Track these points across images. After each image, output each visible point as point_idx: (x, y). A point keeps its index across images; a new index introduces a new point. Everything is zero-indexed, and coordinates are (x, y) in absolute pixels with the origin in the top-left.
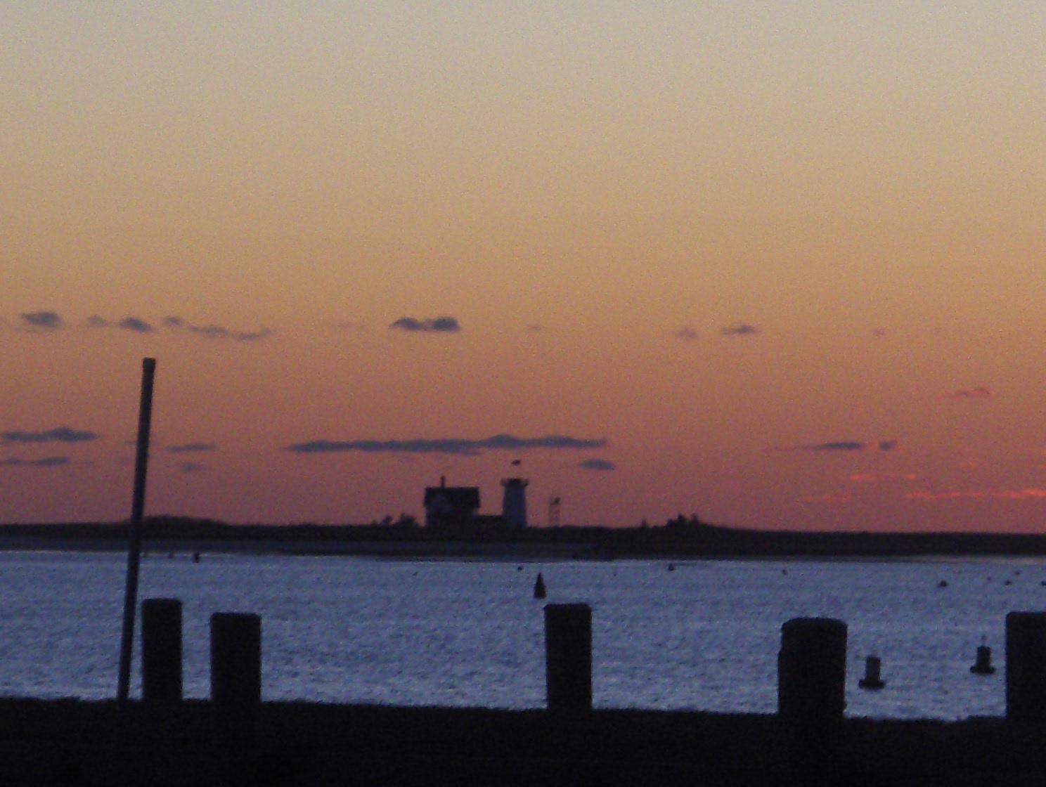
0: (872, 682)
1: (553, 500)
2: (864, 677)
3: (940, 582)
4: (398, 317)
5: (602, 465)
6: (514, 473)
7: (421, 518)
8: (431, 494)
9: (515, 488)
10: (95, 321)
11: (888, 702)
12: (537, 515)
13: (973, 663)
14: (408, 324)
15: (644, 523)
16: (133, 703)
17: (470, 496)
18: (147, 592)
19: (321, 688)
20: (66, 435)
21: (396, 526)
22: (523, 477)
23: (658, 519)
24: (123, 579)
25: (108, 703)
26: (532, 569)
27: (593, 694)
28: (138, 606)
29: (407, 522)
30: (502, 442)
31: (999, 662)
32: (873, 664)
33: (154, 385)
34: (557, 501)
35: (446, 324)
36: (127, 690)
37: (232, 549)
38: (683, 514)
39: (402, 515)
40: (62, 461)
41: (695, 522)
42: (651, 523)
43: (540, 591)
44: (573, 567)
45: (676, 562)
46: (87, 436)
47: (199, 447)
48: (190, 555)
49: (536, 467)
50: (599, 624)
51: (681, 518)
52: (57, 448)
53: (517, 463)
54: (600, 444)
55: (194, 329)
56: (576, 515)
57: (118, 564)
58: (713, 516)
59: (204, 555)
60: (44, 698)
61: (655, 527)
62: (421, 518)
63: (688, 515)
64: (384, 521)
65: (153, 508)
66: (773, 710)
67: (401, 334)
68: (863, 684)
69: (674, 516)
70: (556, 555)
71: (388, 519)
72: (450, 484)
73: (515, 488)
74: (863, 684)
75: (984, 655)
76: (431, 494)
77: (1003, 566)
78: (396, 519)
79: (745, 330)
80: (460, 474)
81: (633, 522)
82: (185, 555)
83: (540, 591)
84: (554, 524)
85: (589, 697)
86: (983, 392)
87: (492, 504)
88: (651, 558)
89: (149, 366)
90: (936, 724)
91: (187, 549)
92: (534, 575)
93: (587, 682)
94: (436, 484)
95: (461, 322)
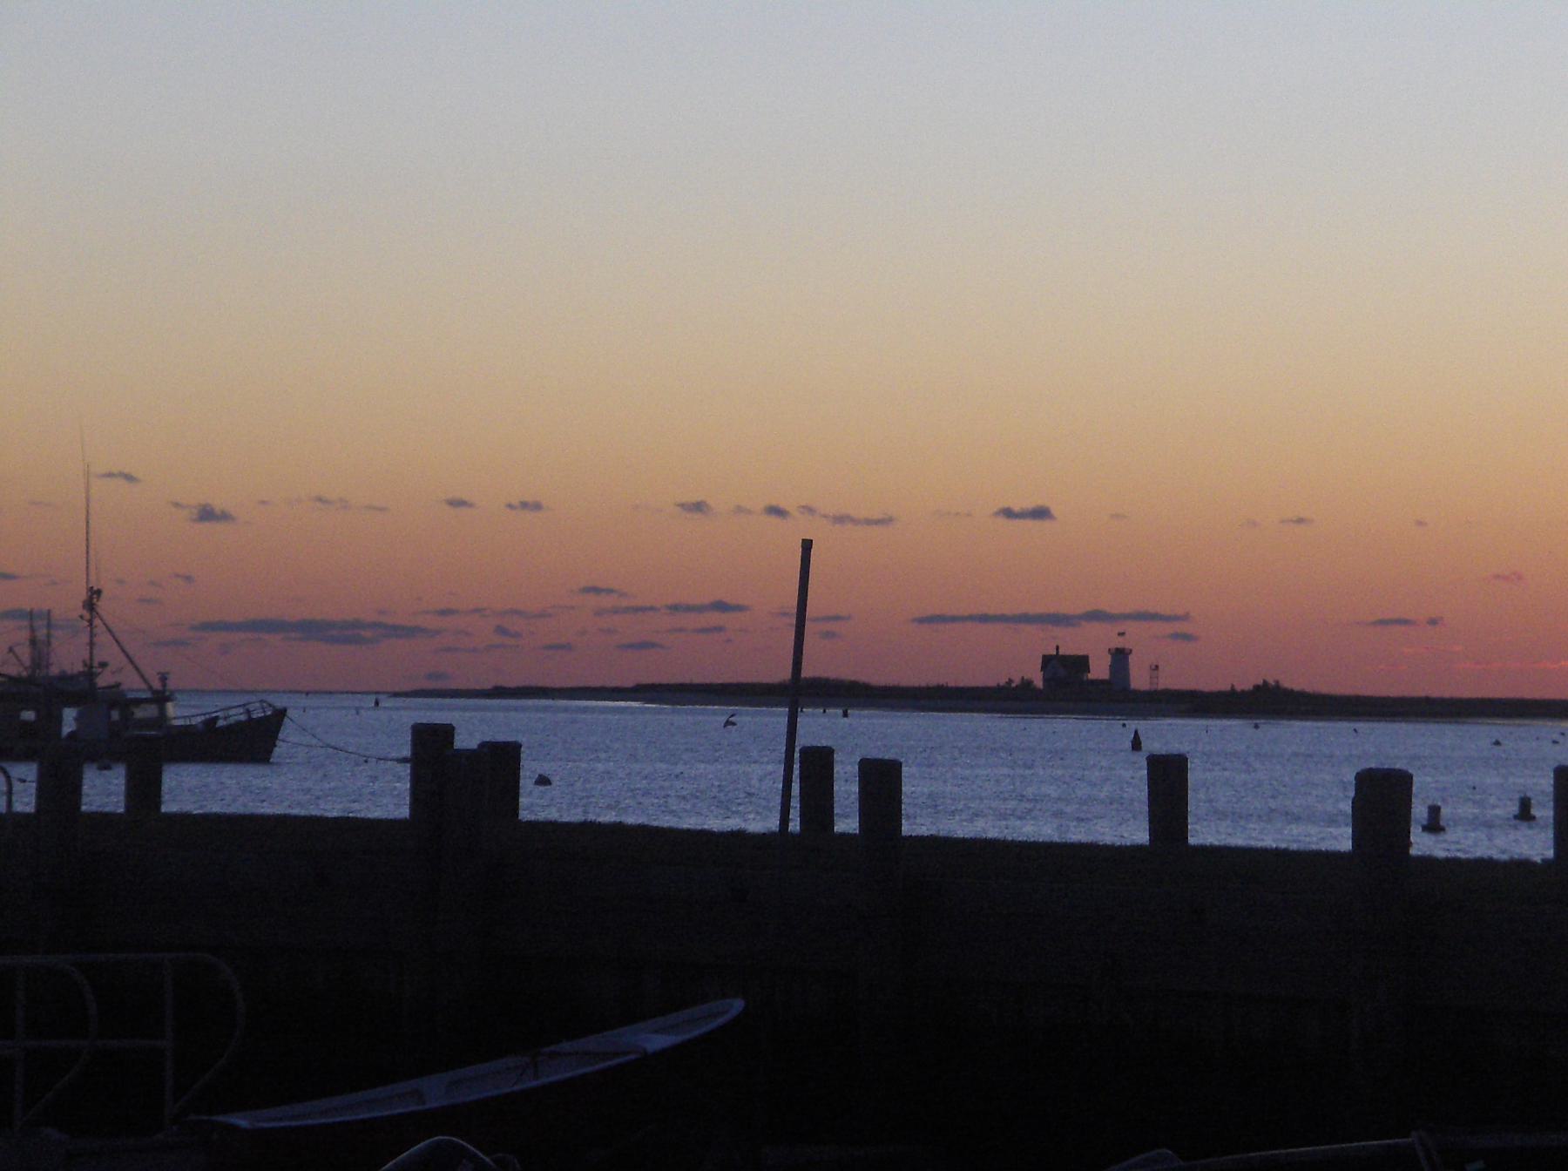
0: (1434, 825)
1: (1153, 667)
3: (1494, 740)
5: (1187, 637)
6: (1119, 643)
7: (1039, 683)
8: (1047, 661)
9: (1120, 657)
10: (739, 510)
12: (1139, 680)
14: (1008, 513)
17: (1082, 663)
18: (802, 741)
19: (356, 806)
20: (721, 606)
22: (1127, 647)
23: (1245, 684)
24: (784, 729)
25: (763, 839)
26: (1133, 724)
28: (797, 755)
29: (1027, 684)
30: (1096, 616)
31: (1544, 812)
32: (1434, 811)
34: (1157, 667)
35: (1041, 513)
37: (879, 707)
39: (1023, 678)
40: (720, 629)
42: (1239, 688)
43: (1136, 745)
44: (1170, 724)
45: (1262, 721)
46: (739, 608)
47: (837, 618)
48: (840, 711)
49: (1138, 638)
50: (1196, 775)
52: (715, 618)
53: (1121, 634)
54: (1185, 617)
55: (825, 516)
56: (1170, 680)
57: (777, 718)
61: (1243, 691)
62: (1039, 683)
63: (1271, 682)
65: (807, 672)
66: (121, 810)
67: (1002, 521)
69: (1260, 682)
70: (1145, 715)
71: (1011, 681)
73: (1120, 657)
74: (1426, 828)
76: (1047, 661)
78: (1017, 682)
79: (1300, 521)
80: (1071, 643)
81: (1223, 686)
82: (542, 716)
83: (1136, 745)
84: (1154, 687)
87: (1100, 669)
88: (1243, 718)
89: (807, 546)
91: (836, 706)
95: (1055, 511)
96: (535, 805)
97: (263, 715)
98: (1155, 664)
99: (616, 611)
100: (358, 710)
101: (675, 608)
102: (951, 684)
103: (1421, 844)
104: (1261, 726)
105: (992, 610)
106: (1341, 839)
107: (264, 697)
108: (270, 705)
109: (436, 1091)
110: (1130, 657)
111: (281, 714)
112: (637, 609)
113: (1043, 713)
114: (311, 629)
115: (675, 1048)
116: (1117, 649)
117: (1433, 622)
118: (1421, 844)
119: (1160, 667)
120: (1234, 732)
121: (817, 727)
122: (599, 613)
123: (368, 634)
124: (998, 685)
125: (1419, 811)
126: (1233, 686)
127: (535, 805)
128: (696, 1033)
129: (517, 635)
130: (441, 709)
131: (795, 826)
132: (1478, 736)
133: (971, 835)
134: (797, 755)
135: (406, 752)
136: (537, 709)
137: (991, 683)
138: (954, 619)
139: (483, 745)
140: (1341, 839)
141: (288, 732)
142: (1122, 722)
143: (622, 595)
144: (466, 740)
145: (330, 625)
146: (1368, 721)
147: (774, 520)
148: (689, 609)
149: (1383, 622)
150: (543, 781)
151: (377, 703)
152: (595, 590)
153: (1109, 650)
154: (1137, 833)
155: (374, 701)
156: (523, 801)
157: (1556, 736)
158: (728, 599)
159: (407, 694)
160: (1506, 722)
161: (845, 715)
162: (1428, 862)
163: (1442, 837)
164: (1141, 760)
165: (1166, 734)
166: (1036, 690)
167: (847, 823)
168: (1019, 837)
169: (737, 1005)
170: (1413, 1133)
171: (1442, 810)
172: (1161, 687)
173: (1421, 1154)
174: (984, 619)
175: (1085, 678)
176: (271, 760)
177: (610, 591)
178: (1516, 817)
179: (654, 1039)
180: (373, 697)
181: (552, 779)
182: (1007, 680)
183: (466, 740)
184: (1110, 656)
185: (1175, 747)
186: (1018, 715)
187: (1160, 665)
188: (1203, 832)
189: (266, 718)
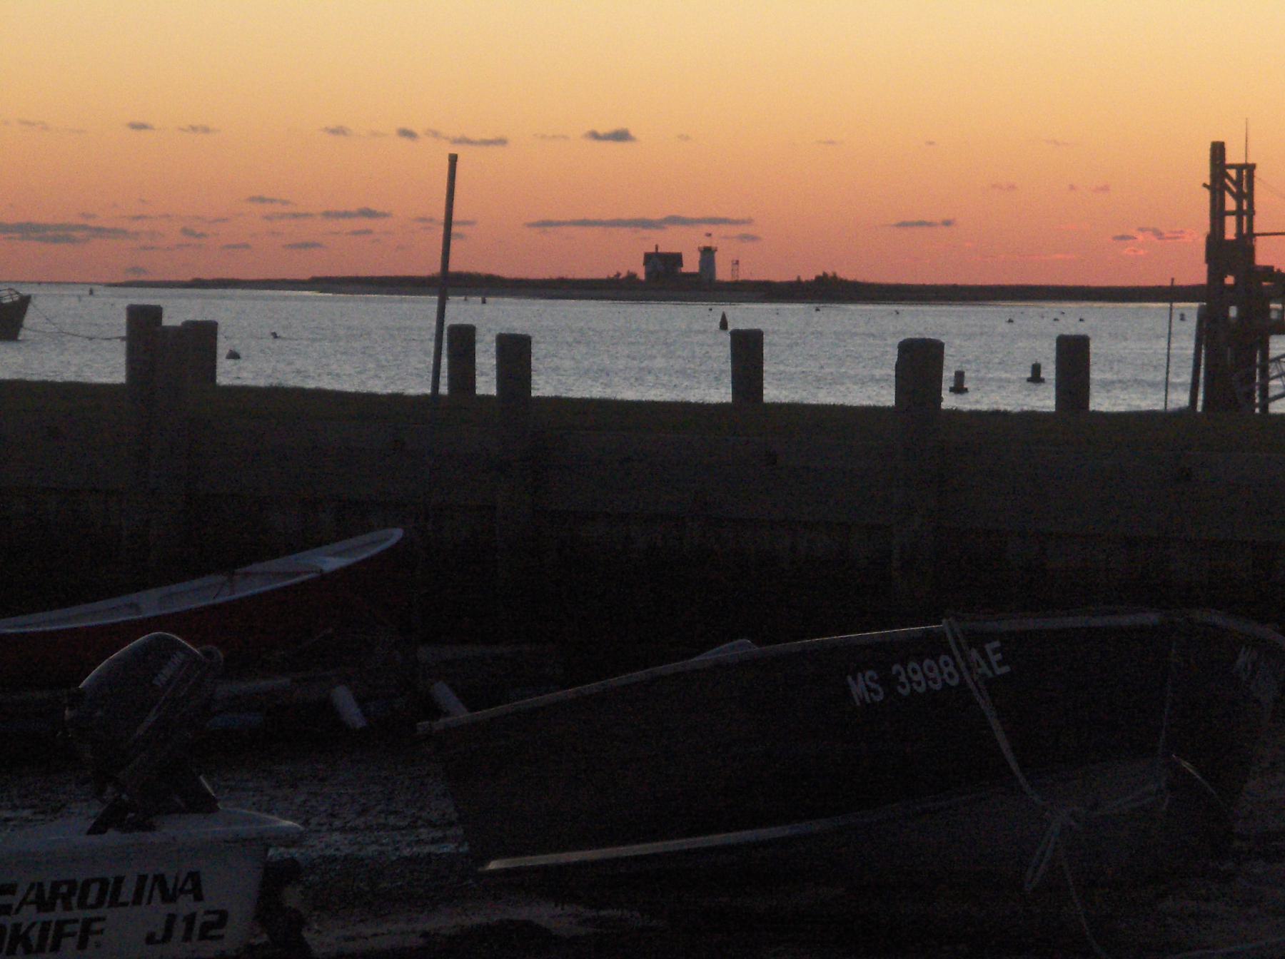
0: (959, 389)
2: (953, 386)
4: (588, 129)
5: (754, 238)
6: (707, 242)
7: (642, 275)
8: (648, 258)
9: (708, 254)
10: (375, 134)
12: (723, 273)
13: (1029, 375)
14: (595, 136)
15: (799, 277)
16: (442, 397)
17: (676, 259)
20: (368, 213)
21: (623, 279)
22: (714, 245)
23: (808, 275)
24: (434, 316)
25: (419, 400)
26: (720, 309)
28: (445, 332)
29: (632, 277)
31: (1049, 372)
32: (960, 376)
34: (737, 262)
35: (621, 136)
36: (438, 388)
38: (826, 271)
39: (628, 272)
40: (368, 232)
41: (835, 277)
42: (803, 279)
43: (724, 325)
45: (822, 305)
46: (384, 215)
51: (825, 275)
52: (365, 223)
54: (749, 222)
55: (447, 138)
57: (428, 304)
58: (848, 272)
59: (489, 299)
62: (642, 275)
63: (830, 273)
64: (615, 276)
65: (454, 267)
68: (952, 390)
69: (821, 274)
71: (619, 274)
72: (662, 250)
73: (708, 254)
74: (952, 390)
75: (1036, 369)
76: (648, 258)
77: (1052, 308)
78: (624, 275)
80: (669, 242)
83: (724, 325)
85: (761, 394)
86: (1012, 187)
87: (691, 265)
89: (453, 159)
90: (1005, 414)
91: (476, 294)
93: (761, 388)
94: (653, 250)
95: (633, 133)
96: (227, 374)
97: (11, 300)
98: (736, 259)
99: (283, 216)
100: (80, 297)
101: (327, 215)
102: (570, 277)
103: (949, 401)
104: (821, 309)
105: (592, 217)
106: (886, 397)
107: (13, 286)
108: (17, 293)
109: (150, 603)
110: (716, 254)
111: (25, 301)
112: (295, 216)
114: (27, 230)
115: (347, 570)
117: (947, 223)
118: (949, 401)
119: (740, 263)
120: (794, 314)
121: (461, 311)
122: (269, 218)
123: (77, 234)
125: (948, 376)
127: (227, 374)
128: (365, 555)
129: (202, 235)
130: (155, 297)
131: (444, 390)
132: (991, 316)
133: (662, 400)
134: (445, 332)
135: (124, 333)
136: (296, 298)
137: (604, 276)
138: (559, 224)
139: (187, 323)
140: (886, 397)
141: (30, 319)
142: (709, 307)
143: (285, 203)
144: (172, 319)
145: (45, 227)
146: (910, 304)
147: (405, 141)
148: (346, 215)
149: (904, 225)
150: (234, 355)
151: (91, 292)
152: (262, 200)
154: (722, 394)
155: (88, 289)
156: (219, 370)
157: (1055, 315)
158: (372, 207)
159: (116, 285)
162: (955, 414)
163: (965, 396)
164: (726, 338)
165: (745, 316)
166: (639, 282)
167: (486, 385)
168: (643, 396)
169: (397, 534)
170: (944, 621)
171: (966, 374)
172: (741, 278)
173: (949, 636)
174: (585, 223)
176: (20, 338)
177: (272, 201)
178: (1029, 380)
179: (330, 561)
180: (88, 287)
181: (241, 356)
183: (172, 319)
184: (699, 254)
185: (1080, 329)
187: (740, 260)
188: (543, 386)
189: (14, 303)
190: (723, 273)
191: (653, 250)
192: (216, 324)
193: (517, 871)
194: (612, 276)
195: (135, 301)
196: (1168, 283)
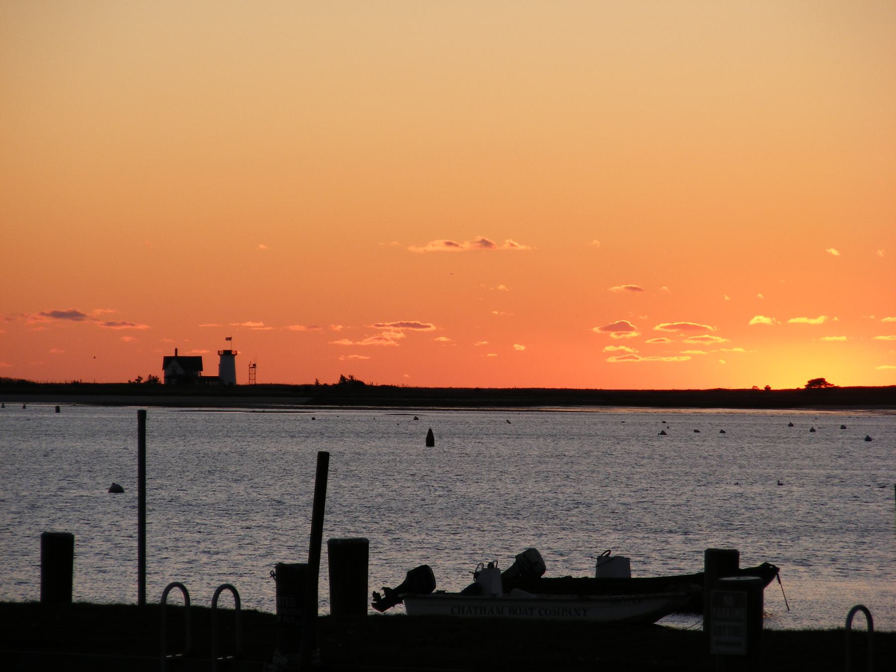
1: (252, 366)
7: (162, 380)
8: (168, 361)
9: (227, 357)
11: (695, 421)
12: (242, 378)
15: (317, 383)
17: (196, 363)
27: (853, 620)
28: (325, 548)
29: (153, 381)
33: (491, 388)
34: (255, 365)
50: (332, 459)
60: (792, 630)
62: (162, 380)
64: (136, 380)
71: (140, 378)
73: (227, 357)
76: (168, 361)
87: (211, 368)
92: (311, 448)
113: (86, 404)
116: (225, 351)
124: (768, 388)
126: (66, 381)
134: (325, 548)
146: (682, 618)
153: (150, 375)
160: (400, 412)
161: (58, 410)
172: (259, 381)
175: (199, 375)
182: (137, 378)
184: (219, 357)
186: (861, 410)
190: (242, 378)
191: (173, 355)
192: (329, 453)
193: (680, 325)
194: (133, 380)
195: (139, 409)
196: (313, 383)
